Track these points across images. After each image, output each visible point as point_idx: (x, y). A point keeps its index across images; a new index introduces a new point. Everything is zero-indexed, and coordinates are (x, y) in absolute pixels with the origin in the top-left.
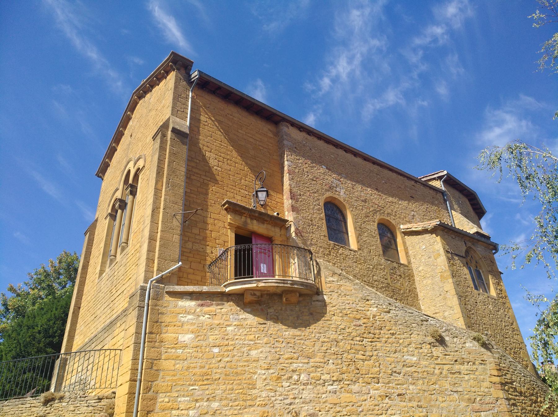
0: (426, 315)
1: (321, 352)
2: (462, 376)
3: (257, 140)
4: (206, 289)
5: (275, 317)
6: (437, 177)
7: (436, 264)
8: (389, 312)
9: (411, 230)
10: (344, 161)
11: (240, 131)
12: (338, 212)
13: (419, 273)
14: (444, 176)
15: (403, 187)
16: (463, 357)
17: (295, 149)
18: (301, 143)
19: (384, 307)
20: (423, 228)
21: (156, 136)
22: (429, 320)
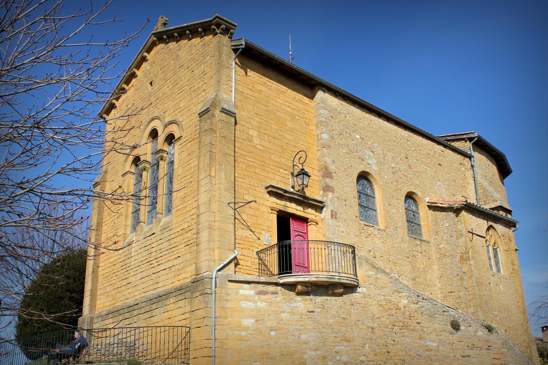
0: (447, 307)
1: (359, 337)
2: (471, 358)
3: (293, 109)
4: (263, 280)
5: (322, 306)
6: (467, 138)
7: (457, 244)
8: (417, 304)
9: (436, 205)
10: (377, 127)
11: (278, 100)
12: (368, 186)
13: (439, 250)
14: (474, 138)
15: (431, 153)
16: (474, 343)
17: (331, 118)
18: (336, 111)
19: (414, 299)
20: (449, 206)
21: (204, 114)
22: (450, 311)
